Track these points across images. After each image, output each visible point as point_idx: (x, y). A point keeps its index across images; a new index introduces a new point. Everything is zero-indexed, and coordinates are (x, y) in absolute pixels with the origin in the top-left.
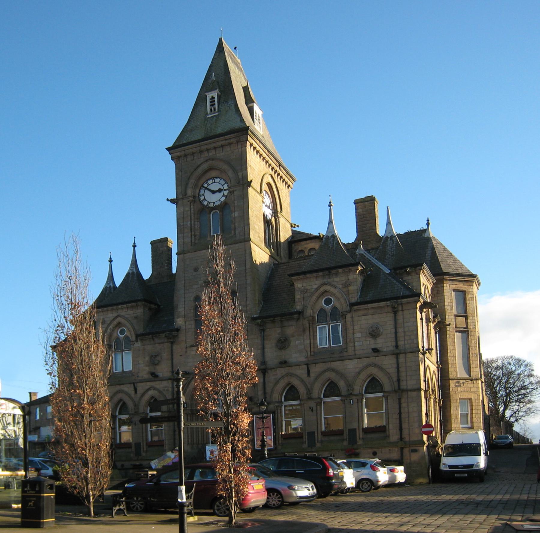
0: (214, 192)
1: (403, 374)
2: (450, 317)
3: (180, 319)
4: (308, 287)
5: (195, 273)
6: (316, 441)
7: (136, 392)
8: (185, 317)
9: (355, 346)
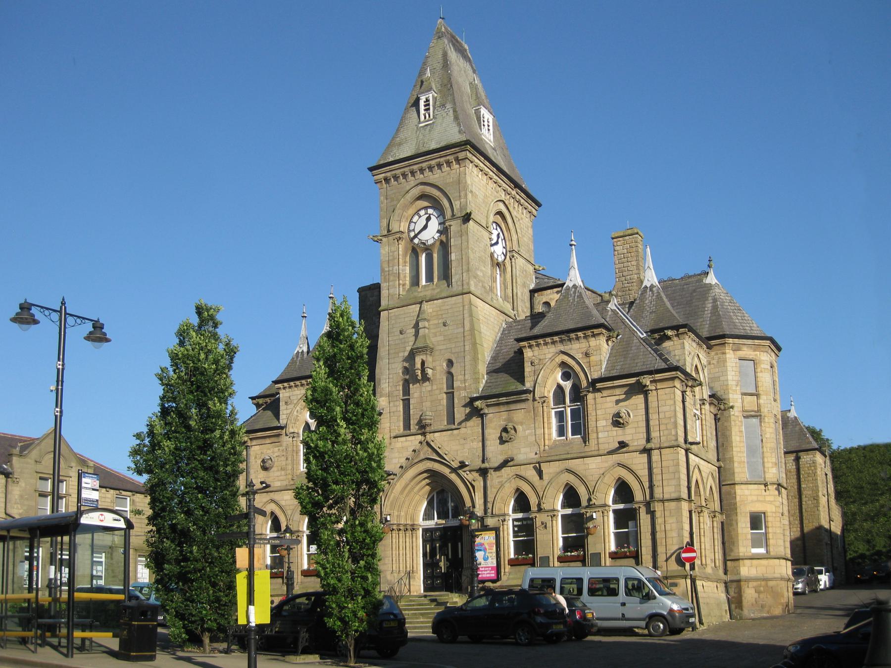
0: (425, 227)
1: (657, 478)
2: (735, 396)
7: (541, 477)
8: (389, 395)
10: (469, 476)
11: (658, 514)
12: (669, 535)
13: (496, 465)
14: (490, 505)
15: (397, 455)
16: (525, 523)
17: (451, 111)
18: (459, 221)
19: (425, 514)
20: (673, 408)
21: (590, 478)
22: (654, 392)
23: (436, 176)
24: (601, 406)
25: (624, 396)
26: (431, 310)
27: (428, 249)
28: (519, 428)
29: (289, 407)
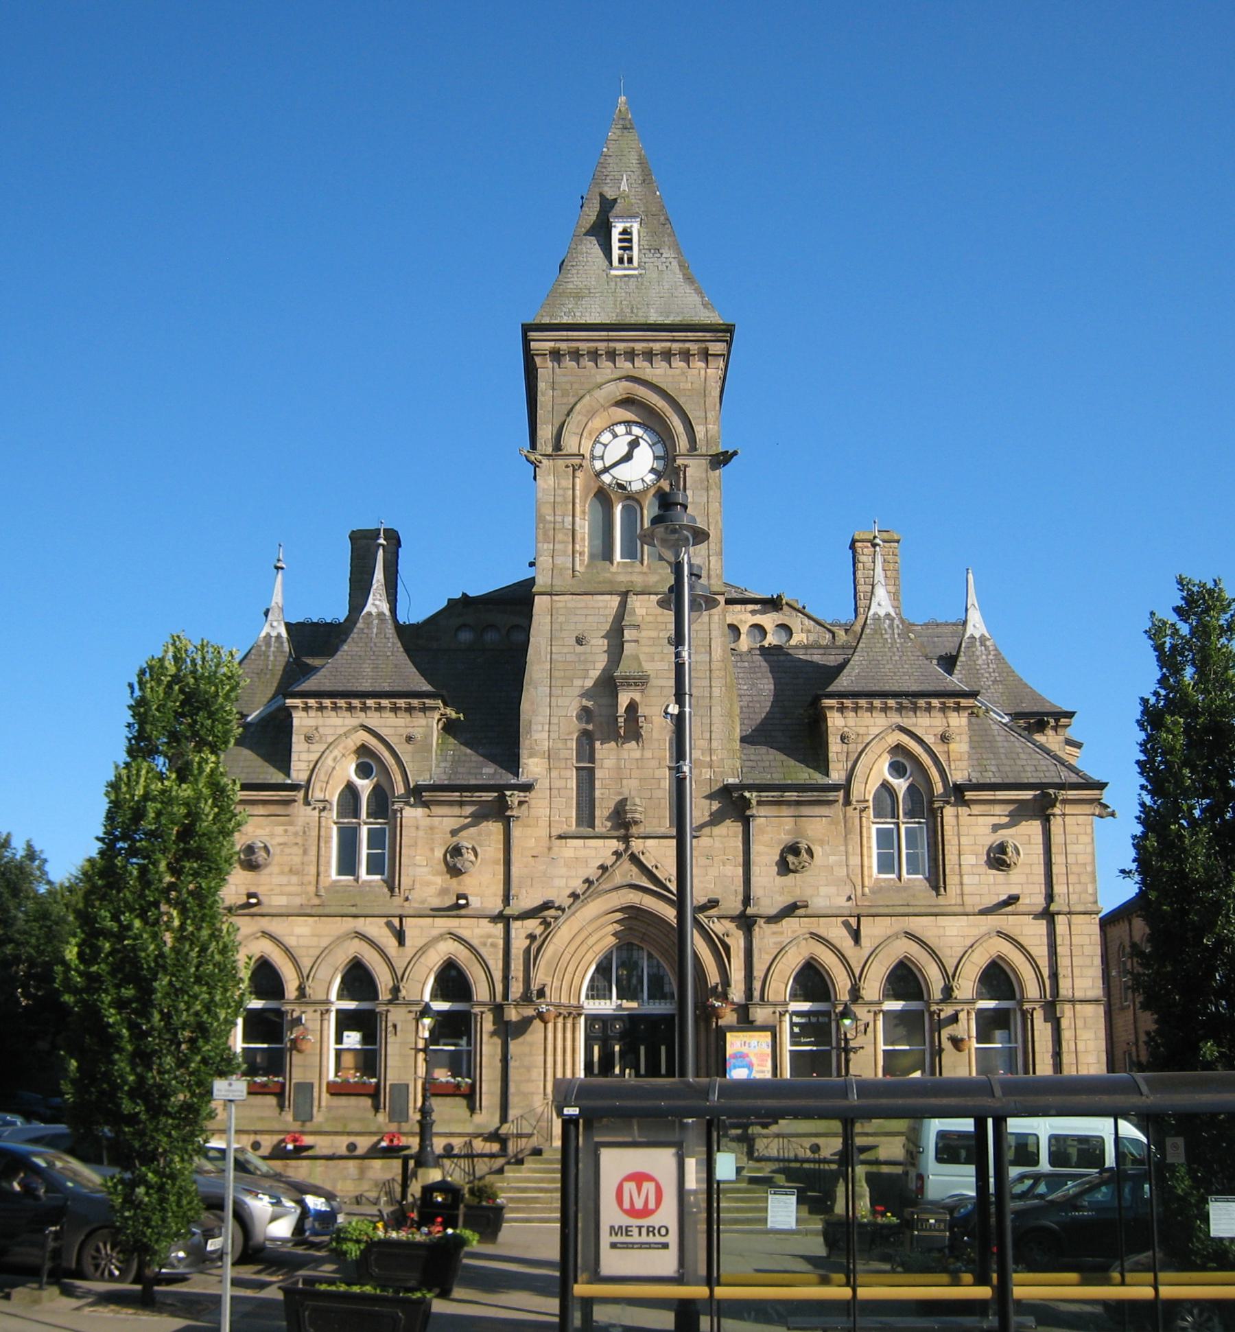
0: (628, 457)
1: (1063, 962)
3: (536, 760)
5: (579, 649)
6: (315, 1109)
9: (962, 884)
10: (718, 927)
11: (1064, 1023)
12: (1082, 1058)
13: (773, 911)
14: (757, 985)
15: (563, 871)
16: (813, 1019)
17: (675, 264)
18: (704, 462)
19: (591, 987)
20: (1089, 849)
21: (948, 952)
22: (1059, 819)
23: (658, 372)
24: (969, 832)
25: (1007, 819)
26: (644, 611)
27: (632, 500)
28: (817, 850)
29: (314, 747)
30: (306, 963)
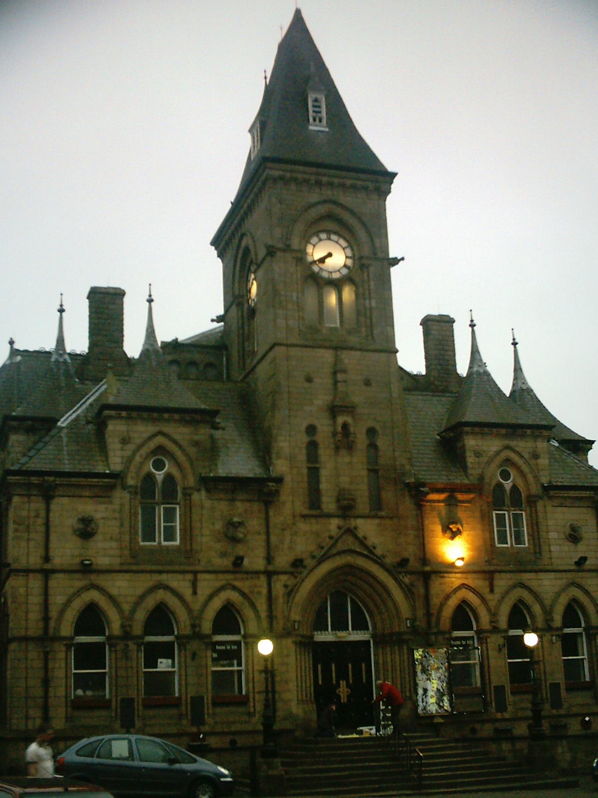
4: (485, 448)
5: (307, 385)
7: (195, 593)
30: (126, 608)
